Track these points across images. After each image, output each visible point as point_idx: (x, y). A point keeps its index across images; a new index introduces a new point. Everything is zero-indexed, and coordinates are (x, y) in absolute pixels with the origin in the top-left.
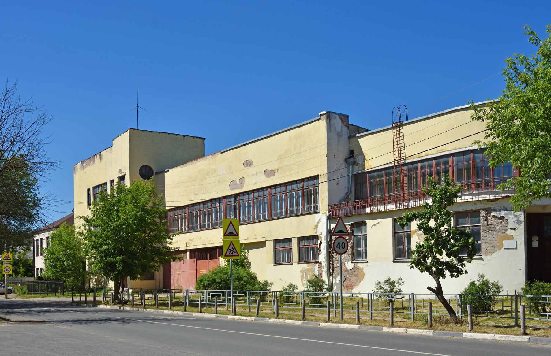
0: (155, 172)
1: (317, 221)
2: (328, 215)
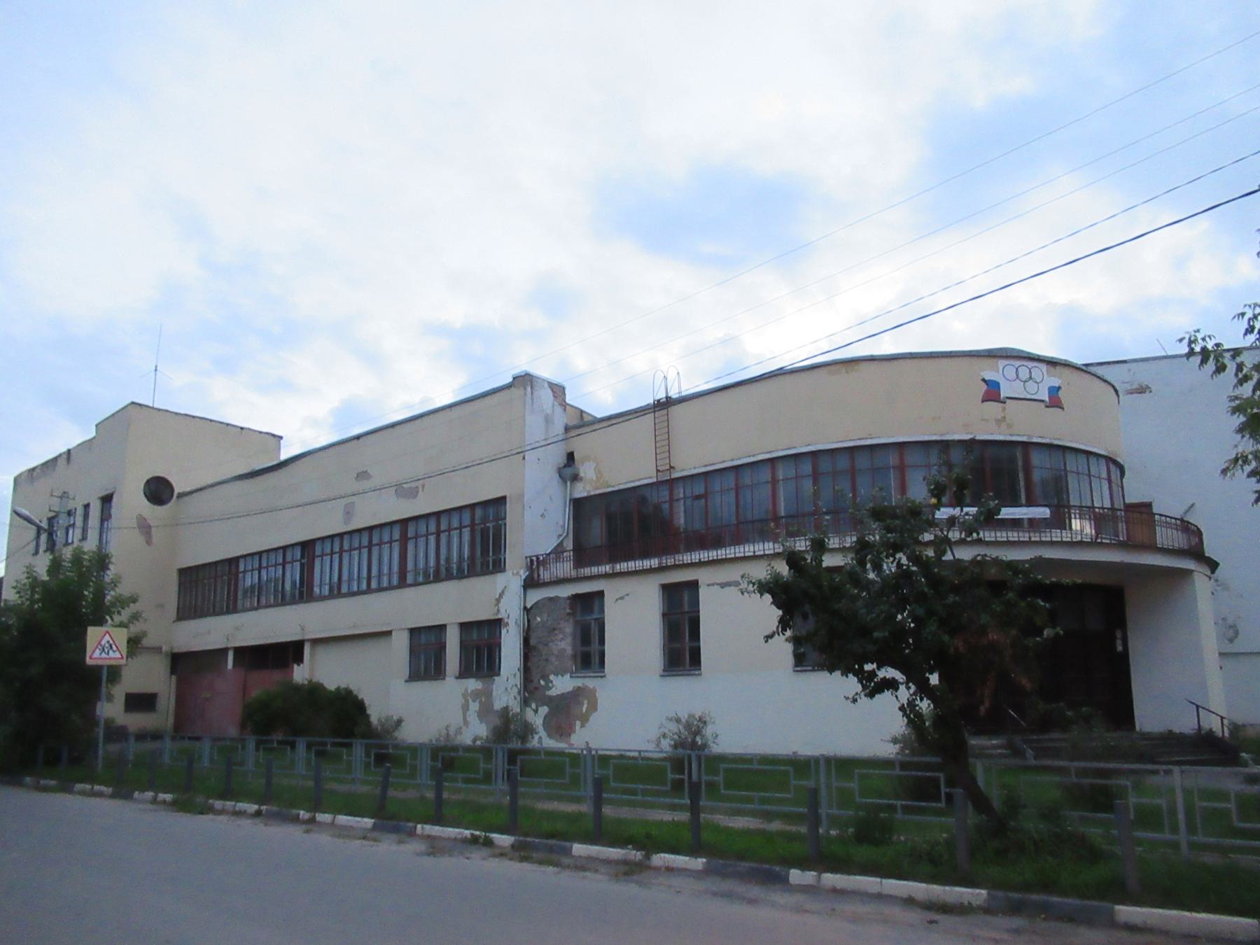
0: (177, 491)
1: (499, 591)
2: (523, 577)
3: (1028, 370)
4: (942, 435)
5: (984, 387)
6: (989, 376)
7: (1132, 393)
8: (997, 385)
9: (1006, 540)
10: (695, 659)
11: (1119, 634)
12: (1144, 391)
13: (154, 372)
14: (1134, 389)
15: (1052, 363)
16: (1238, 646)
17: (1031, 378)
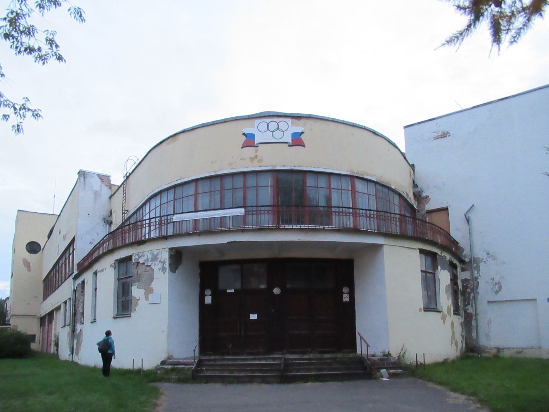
3: (276, 124)
4: (215, 172)
5: (244, 138)
7: (438, 139)
8: (252, 136)
11: (345, 290)
12: (445, 135)
13: (53, 199)
14: (439, 136)
15: (297, 117)
16: (500, 297)
17: (278, 129)
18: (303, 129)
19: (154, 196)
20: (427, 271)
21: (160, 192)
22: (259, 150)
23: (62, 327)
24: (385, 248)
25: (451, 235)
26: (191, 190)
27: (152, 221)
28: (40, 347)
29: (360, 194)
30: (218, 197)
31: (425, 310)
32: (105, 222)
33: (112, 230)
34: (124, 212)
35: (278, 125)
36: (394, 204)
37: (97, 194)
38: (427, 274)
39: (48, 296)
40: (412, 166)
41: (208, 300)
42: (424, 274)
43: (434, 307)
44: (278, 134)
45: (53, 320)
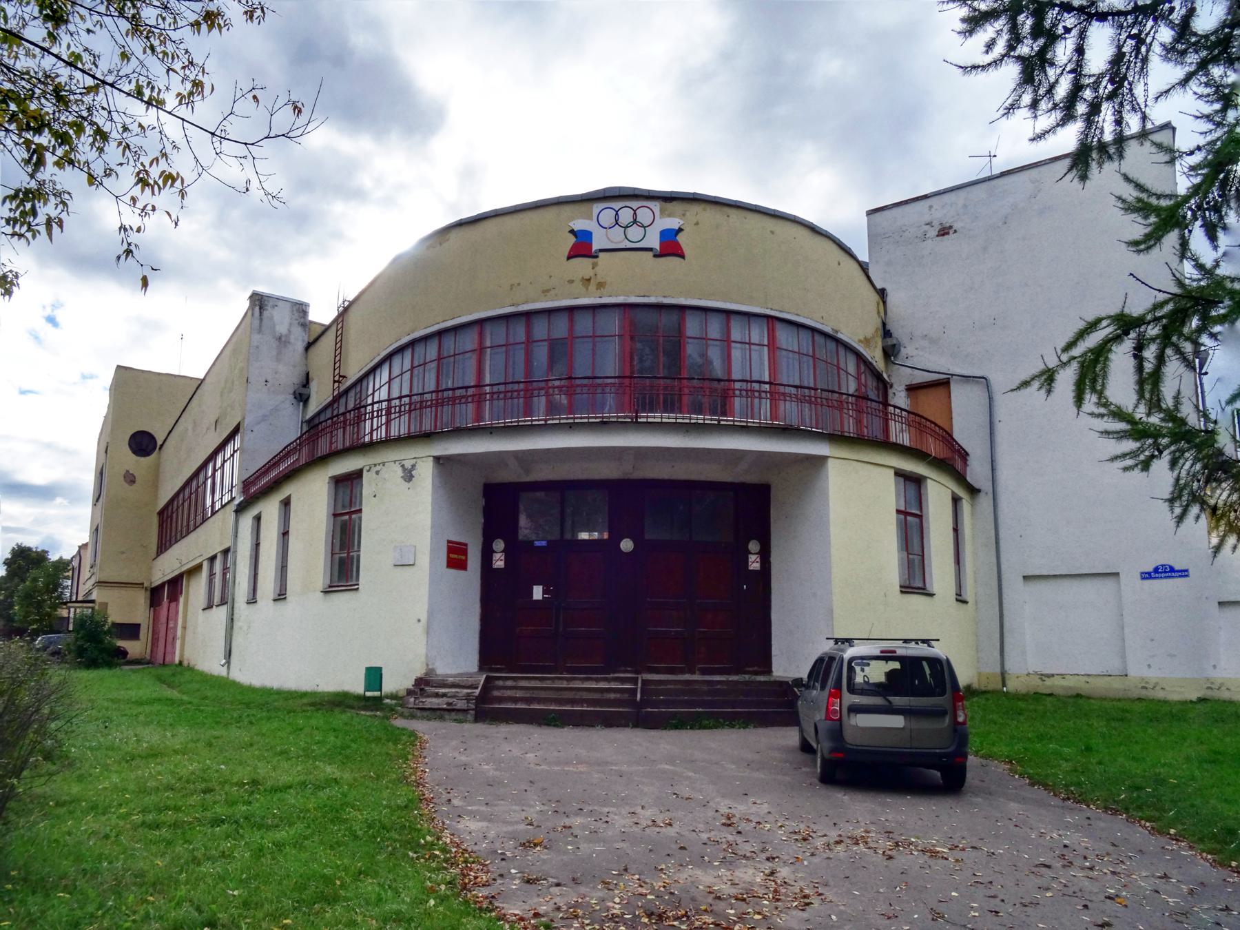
3: (632, 212)
5: (572, 240)
6: (579, 225)
9: (840, 433)
10: (1143, 578)
11: (754, 546)
15: (668, 198)
17: (635, 222)
18: (682, 222)
19: (400, 350)
20: (908, 510)
21: (412, 344)
22: (599, 263)
23: (204, 610)
24: (831, 464)
25: (955, 436)
26: (468, 341)
27: (403, 403)
28: (149, 651)
29: (784, 353)
30: (520, 355)
31: (903, 590)
32: (295, 398)
33: (308, 417)
34: (337, 378)
35: (635, 213)
36: (847, 373)
37: (282, 341)
38: (909, 518)
39: (171, 546)
40: (882, 293)
41: (499, 562)
42: (902, 517)
43: (920, 585)
44: (635, 233)
45: (181, 593)
